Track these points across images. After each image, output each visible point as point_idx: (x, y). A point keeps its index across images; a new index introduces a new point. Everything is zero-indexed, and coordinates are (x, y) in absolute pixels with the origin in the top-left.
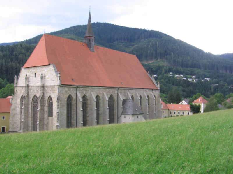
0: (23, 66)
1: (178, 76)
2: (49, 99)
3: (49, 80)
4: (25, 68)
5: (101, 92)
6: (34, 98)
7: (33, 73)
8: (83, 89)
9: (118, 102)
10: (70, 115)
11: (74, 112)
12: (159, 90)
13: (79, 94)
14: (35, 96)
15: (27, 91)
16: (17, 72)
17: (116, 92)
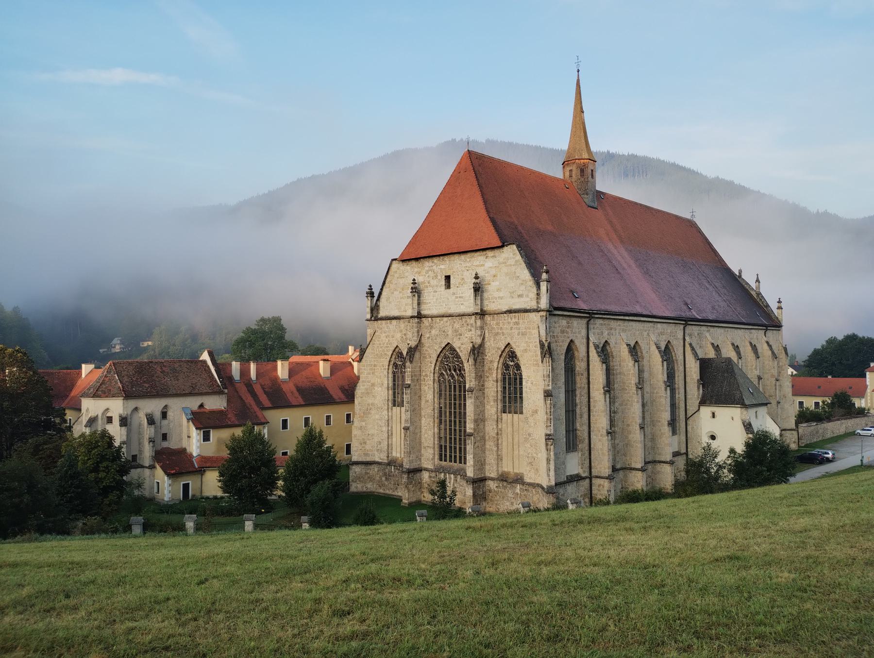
2: (504, 354)
3: (501, 294)
5: (645, 334)
6: (442, 355)
7: (436, 276)
8: (601, 324)
11: (580, 398)
14: (449, 348)
15: (418, 332)
17: (680, 335)
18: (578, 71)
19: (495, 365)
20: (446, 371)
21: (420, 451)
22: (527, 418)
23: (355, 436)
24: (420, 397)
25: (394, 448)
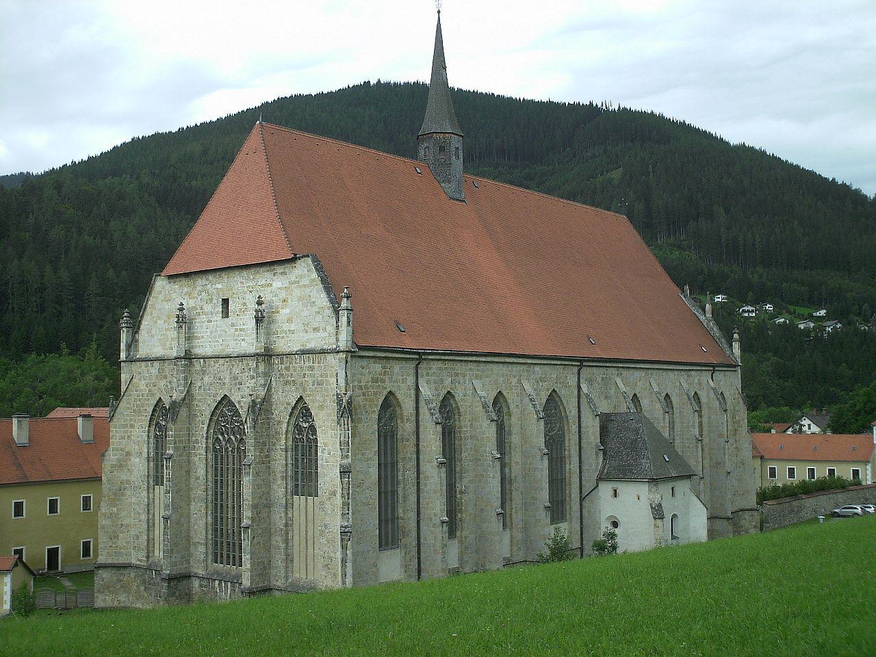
0: (162, 268)
1: (750, 308)
2: (296, 412)
4: (170, 277)
5: (514, 381)
7: (211, 300)
8: (440, 369)
9: (580, 427)
10: (393, 486)
11: (406, 473)
12: (739, 369)
13: (425, 390)
15: (186, 379)
16: (135, 296)
17: (572, 381)
18: (439, 12)
19: (285, 426)
20: (222, 434)
21: (188, 549)
22: (322, 503)
23: (103, 527)
24: (188, 472)
25: (157, 545)
